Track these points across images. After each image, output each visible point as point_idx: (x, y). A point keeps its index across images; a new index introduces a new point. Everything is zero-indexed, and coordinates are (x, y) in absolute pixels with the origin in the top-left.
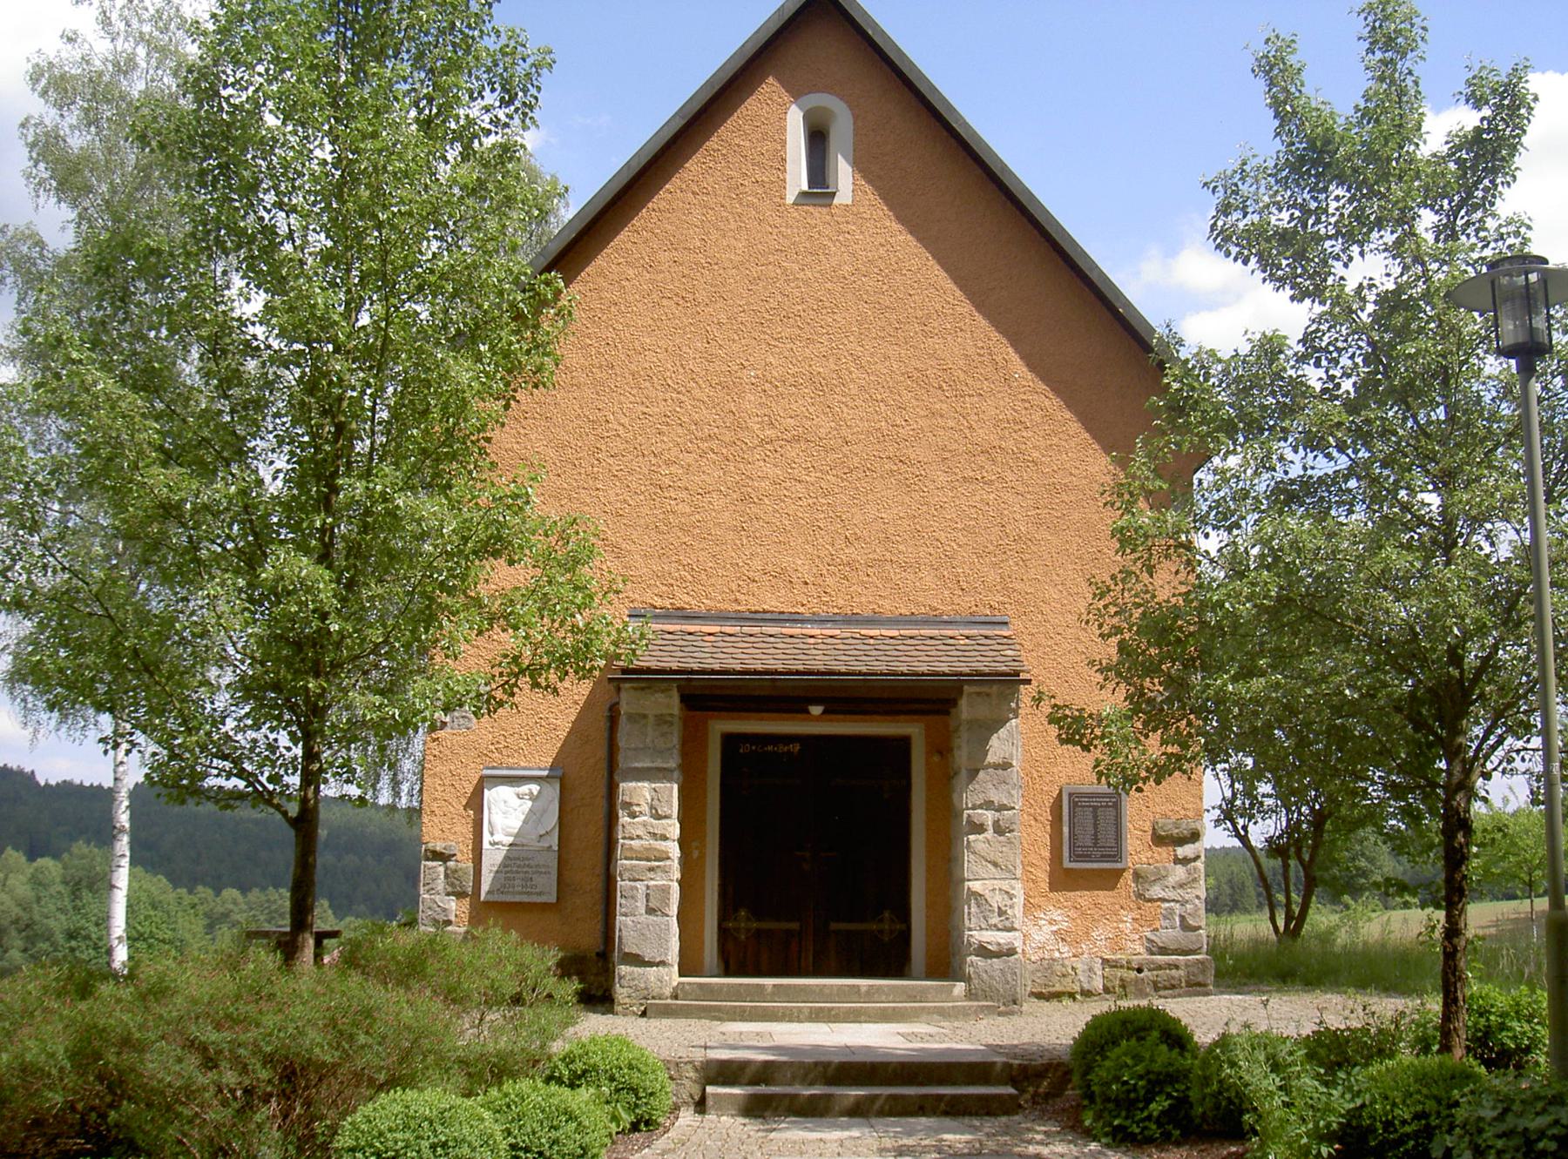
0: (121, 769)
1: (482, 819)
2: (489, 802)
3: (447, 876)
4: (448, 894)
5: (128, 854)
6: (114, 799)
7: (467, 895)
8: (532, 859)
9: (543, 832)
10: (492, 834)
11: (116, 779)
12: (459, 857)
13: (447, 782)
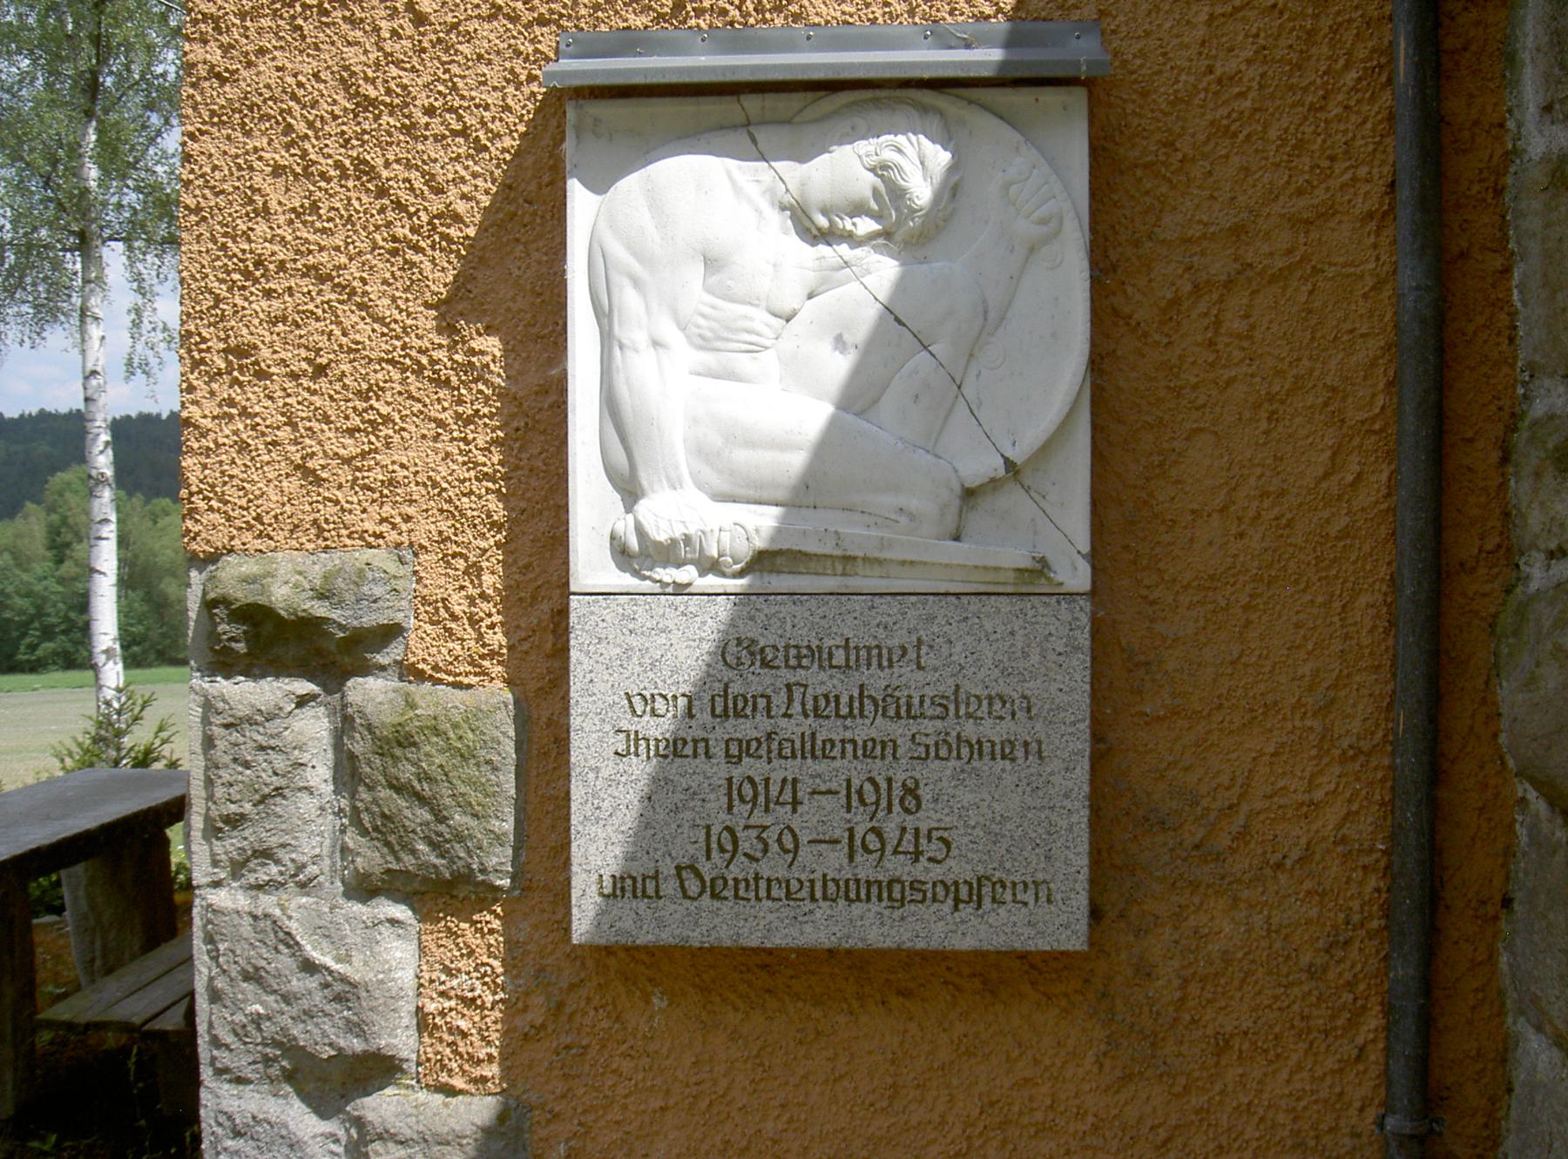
0: (94, 382)
1: (554, 396)
2: (597, 255)
3: (347, 773)
4: (363, 889)
5: (113, 518)
6: (83, 433)
7: (485, 895)
8: (913, 652)
9: (981, 465)
10: (630, 490)
11: (87, 400)
12: (421, 643)
13: (327, 153)
